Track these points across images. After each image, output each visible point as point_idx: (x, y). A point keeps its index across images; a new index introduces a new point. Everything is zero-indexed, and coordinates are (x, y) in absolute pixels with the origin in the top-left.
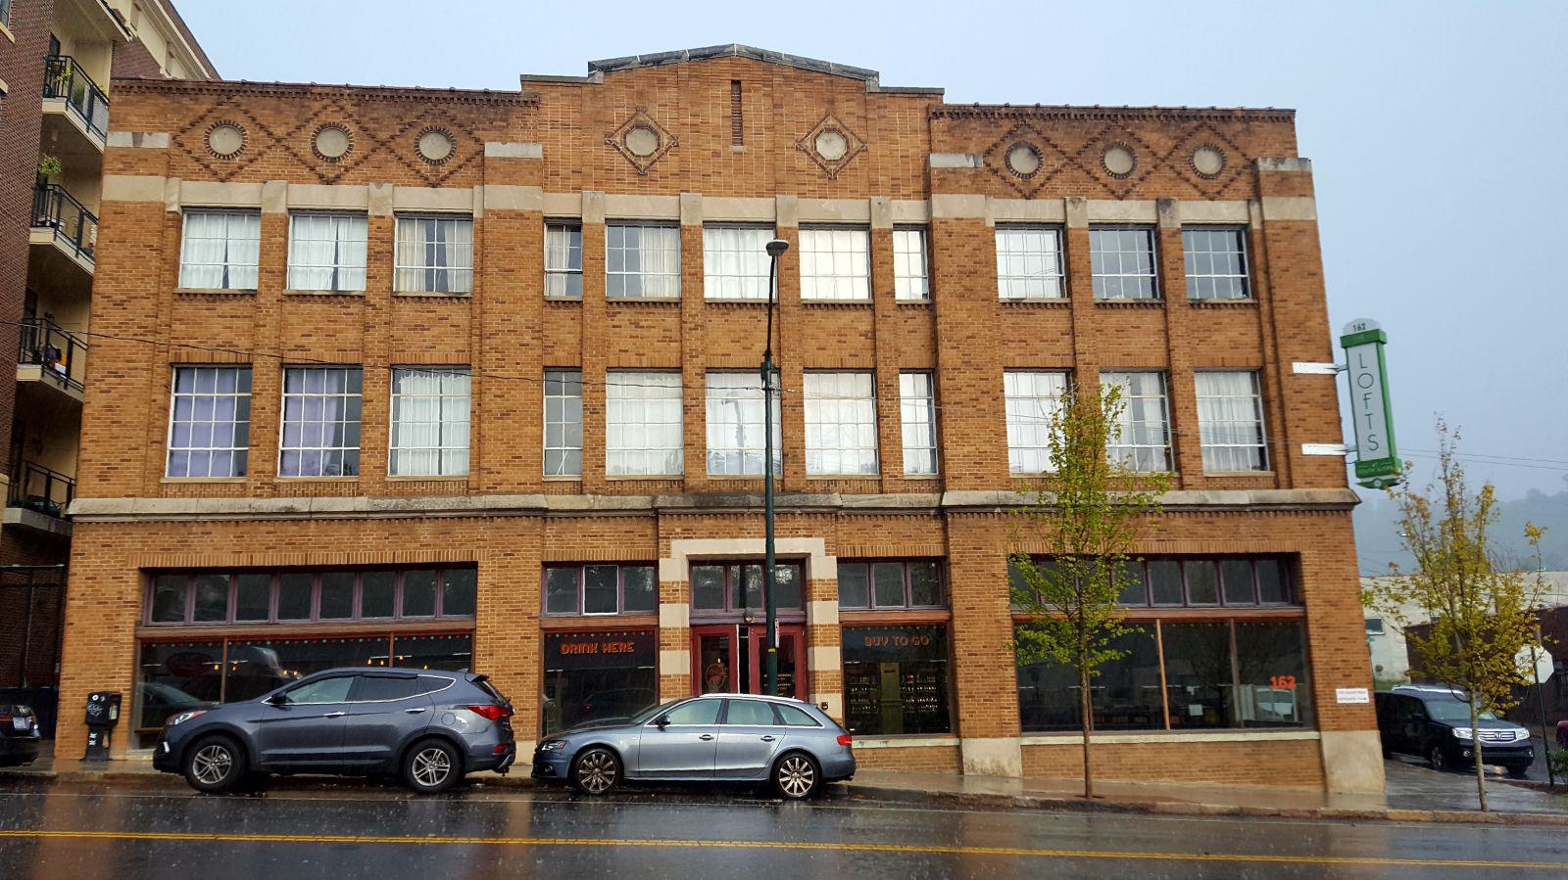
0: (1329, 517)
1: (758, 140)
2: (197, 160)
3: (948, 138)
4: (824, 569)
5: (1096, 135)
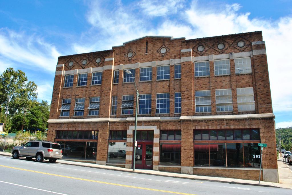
2: (67, 67)
5: (216, 42)
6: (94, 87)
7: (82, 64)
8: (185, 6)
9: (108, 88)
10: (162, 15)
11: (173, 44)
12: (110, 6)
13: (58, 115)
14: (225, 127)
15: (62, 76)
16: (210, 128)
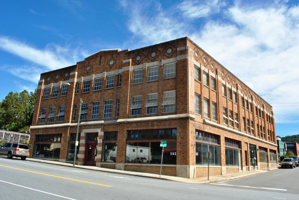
6: (62, 98)
7: (56, 79)
8: (228, 3)
9: (70, 98)
10: (204, 16)
11: (119, 56)
12: (150, 14)
13: (38, 122)
14: (150, 128)
15: (42, 90)
16: (139, 129)
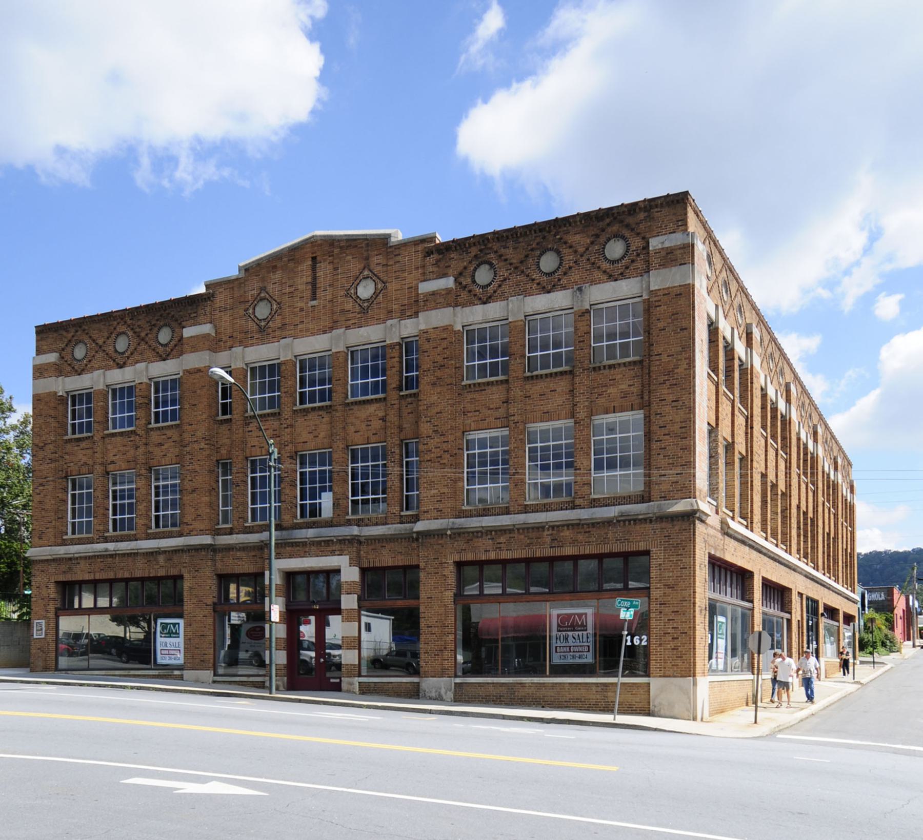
0: (675, 523)
1: (325, 295)
3: (435, 269)
4: (350, 574)
